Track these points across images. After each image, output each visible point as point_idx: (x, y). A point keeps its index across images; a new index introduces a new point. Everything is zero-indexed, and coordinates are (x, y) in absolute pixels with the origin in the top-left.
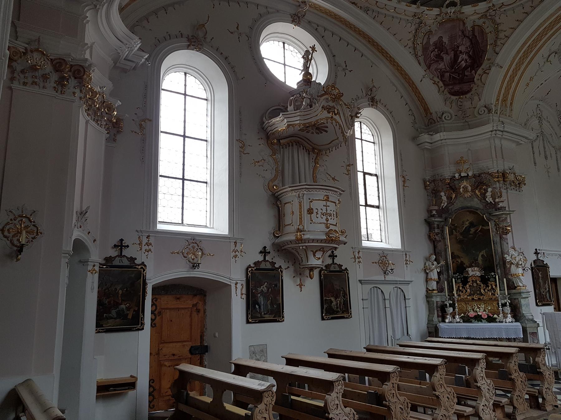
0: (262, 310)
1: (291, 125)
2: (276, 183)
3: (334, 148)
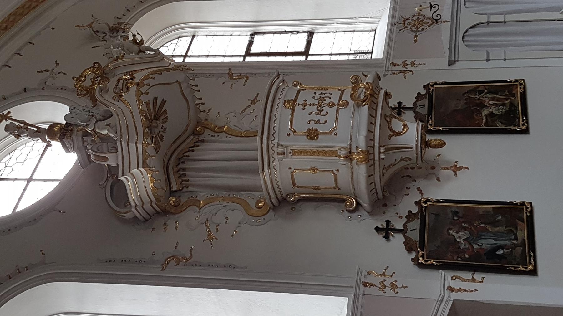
0: (507, 242)
1: (144, 162)
2: (252, 203)
3: (196, 94)
